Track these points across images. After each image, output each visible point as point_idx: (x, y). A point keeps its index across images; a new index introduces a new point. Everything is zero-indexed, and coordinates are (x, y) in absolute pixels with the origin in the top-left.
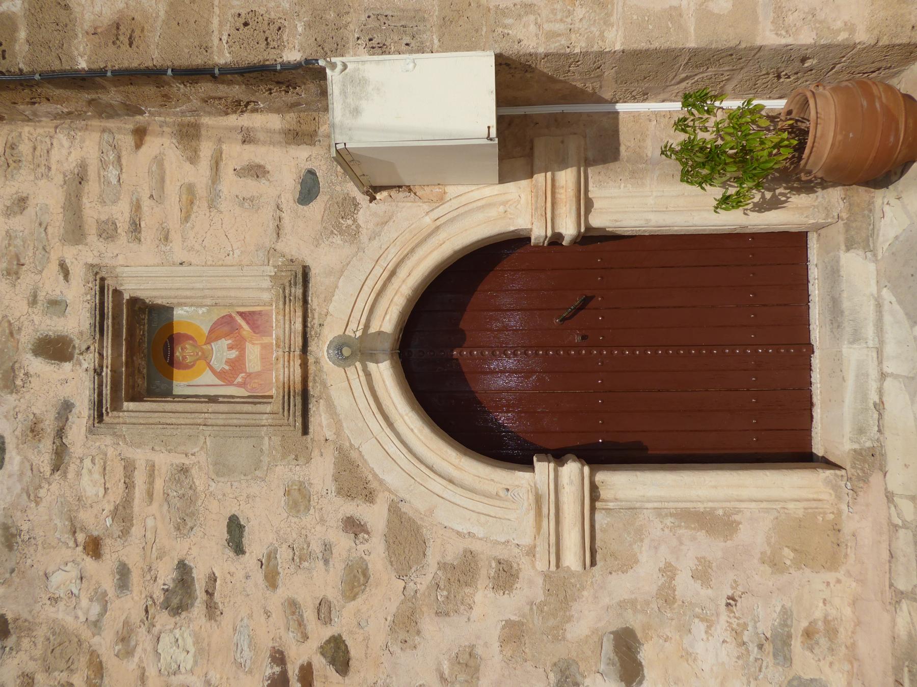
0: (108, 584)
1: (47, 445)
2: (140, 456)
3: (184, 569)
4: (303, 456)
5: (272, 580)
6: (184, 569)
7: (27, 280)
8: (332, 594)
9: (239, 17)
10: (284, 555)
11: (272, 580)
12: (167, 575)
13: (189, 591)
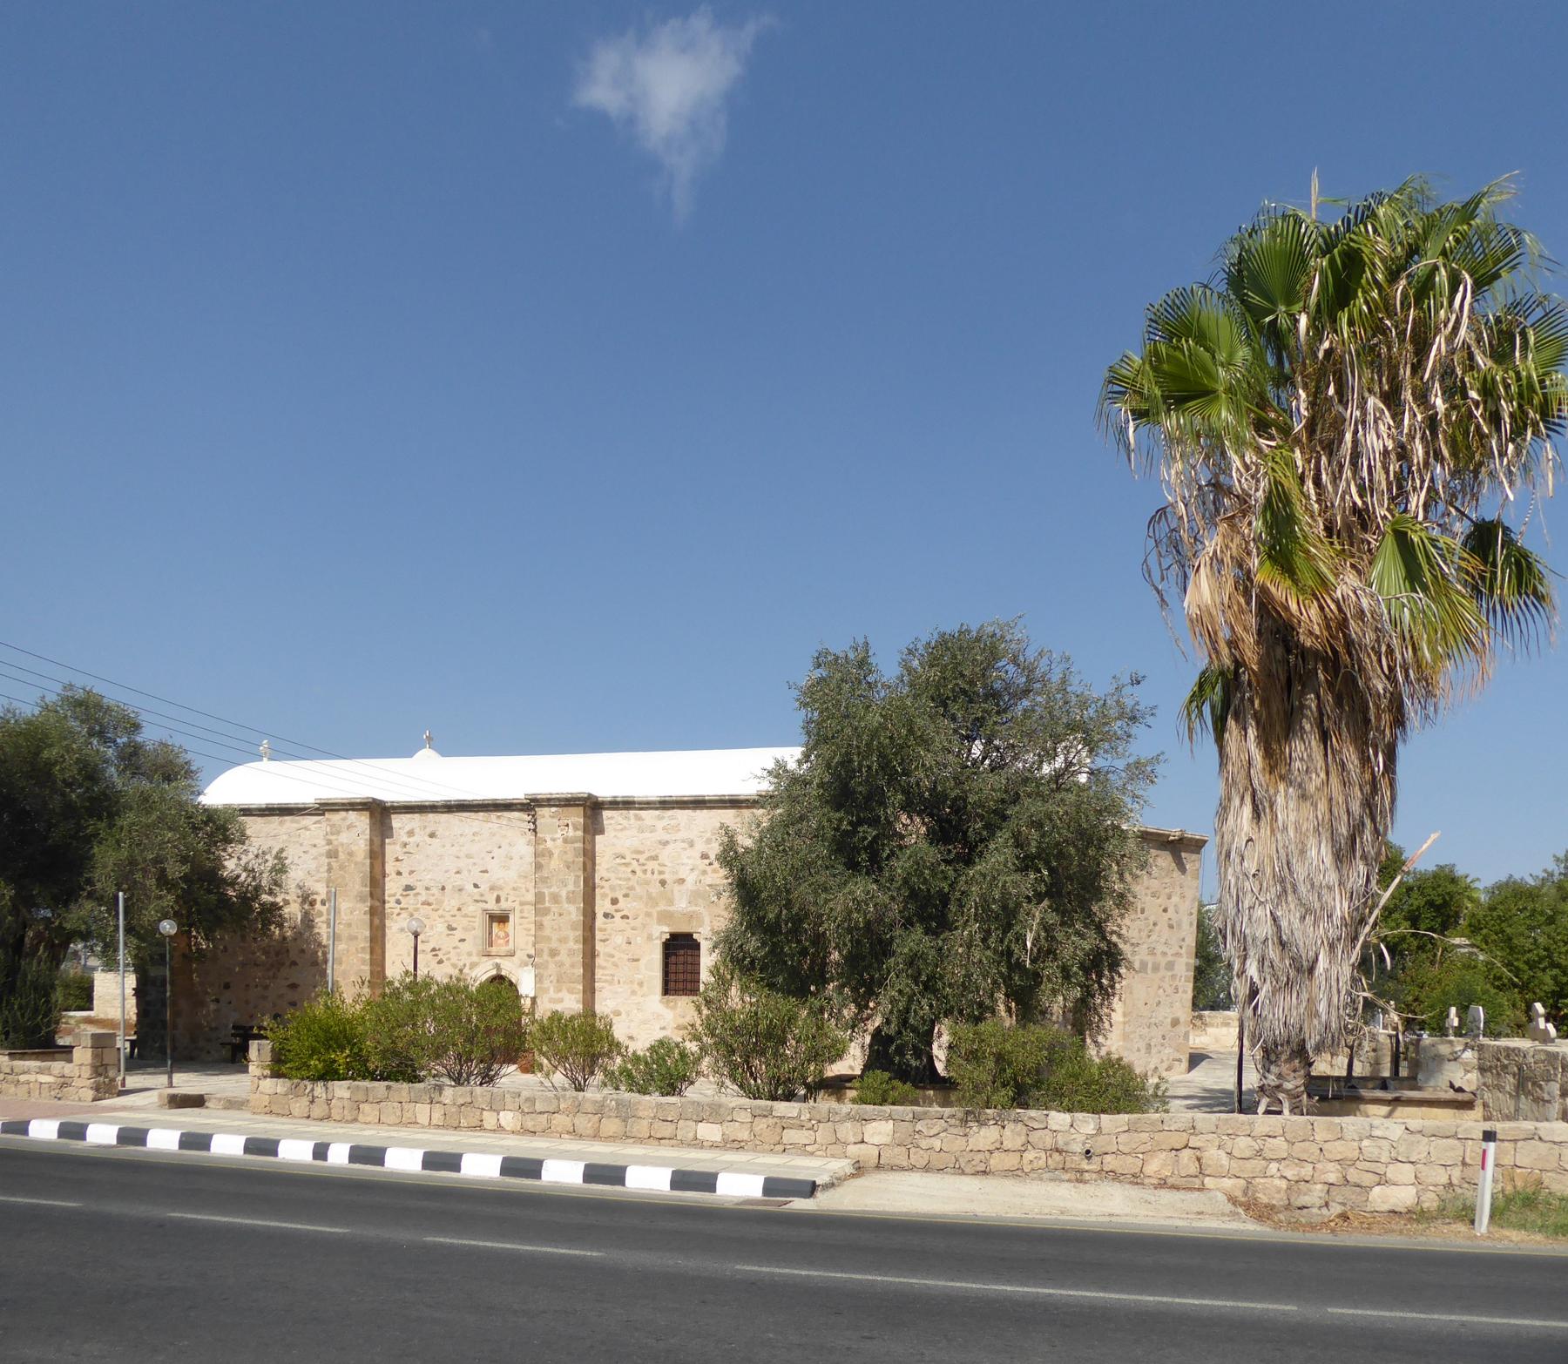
0: (451, 913)
1: (479, 898)
2: (477, 919)
3: (456, 929)
4: (478, 955)
5: (454, 948)
6: (456, 929)
7: (512, 892)
8: (452, 961)
9: (1089, 1158)
10: (458, 950)
11: (454, 948)
12: (454, 925)
13: (306, 907)
